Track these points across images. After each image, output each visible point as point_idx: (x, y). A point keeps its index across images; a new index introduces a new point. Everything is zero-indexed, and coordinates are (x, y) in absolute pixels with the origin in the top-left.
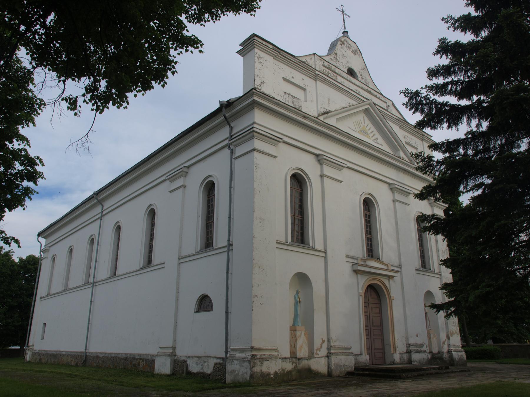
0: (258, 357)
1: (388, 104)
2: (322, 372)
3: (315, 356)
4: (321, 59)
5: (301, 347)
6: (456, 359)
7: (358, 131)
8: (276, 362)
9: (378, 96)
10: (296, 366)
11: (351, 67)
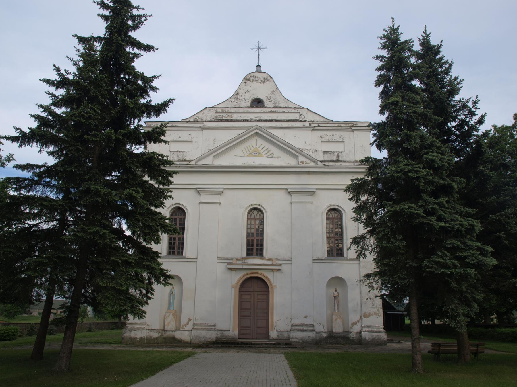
0: (129, 328)
1: (301, 113)
2: (185, 340)
3: (181, 329)
4: (214, 109)
5: (169, 323)
6: (367, 339)
7: (246, 155)
8: (142, 331)
9: (286, 112)
10: (162, 335)
11: (256, 97)
